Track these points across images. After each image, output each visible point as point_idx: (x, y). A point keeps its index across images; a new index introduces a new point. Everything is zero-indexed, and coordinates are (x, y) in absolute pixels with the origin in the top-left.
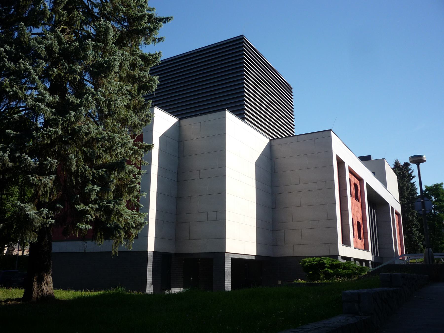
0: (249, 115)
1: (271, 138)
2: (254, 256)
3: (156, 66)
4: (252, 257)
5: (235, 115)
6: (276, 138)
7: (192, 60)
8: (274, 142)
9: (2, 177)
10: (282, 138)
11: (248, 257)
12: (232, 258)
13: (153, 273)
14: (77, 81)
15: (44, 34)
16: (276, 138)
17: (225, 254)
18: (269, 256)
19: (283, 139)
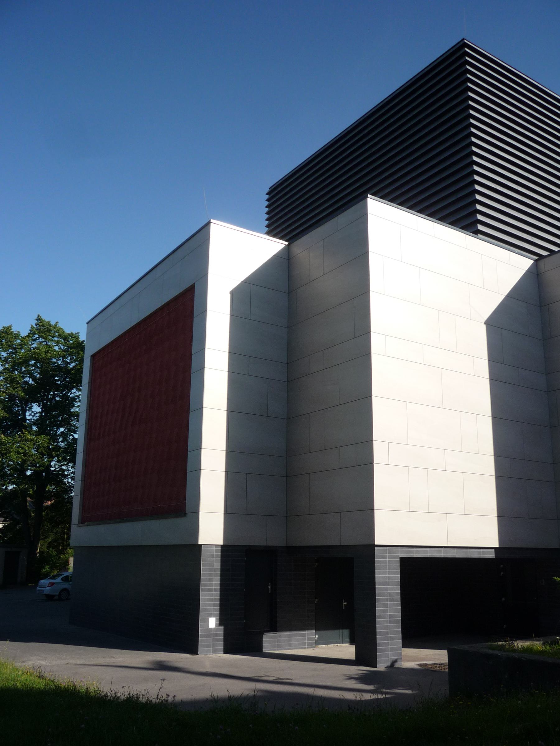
0: (528, 185)
1: (537, 258)
2: (493, 551)
3: (61, 451)
4: (480, 553)
5: (448, 224)
6: (544, 253)
7: (300, 180)
8: (544, 265)
9: (57, 380)
10: (553, 254)
11: (484, 553)
12: (400, 558)
13: (221, 595)
14: (62, 400)
15: (24, 438)
16: (544, 253)
17: (376, 548)
18: (534, 547)
19: (546, 259)
